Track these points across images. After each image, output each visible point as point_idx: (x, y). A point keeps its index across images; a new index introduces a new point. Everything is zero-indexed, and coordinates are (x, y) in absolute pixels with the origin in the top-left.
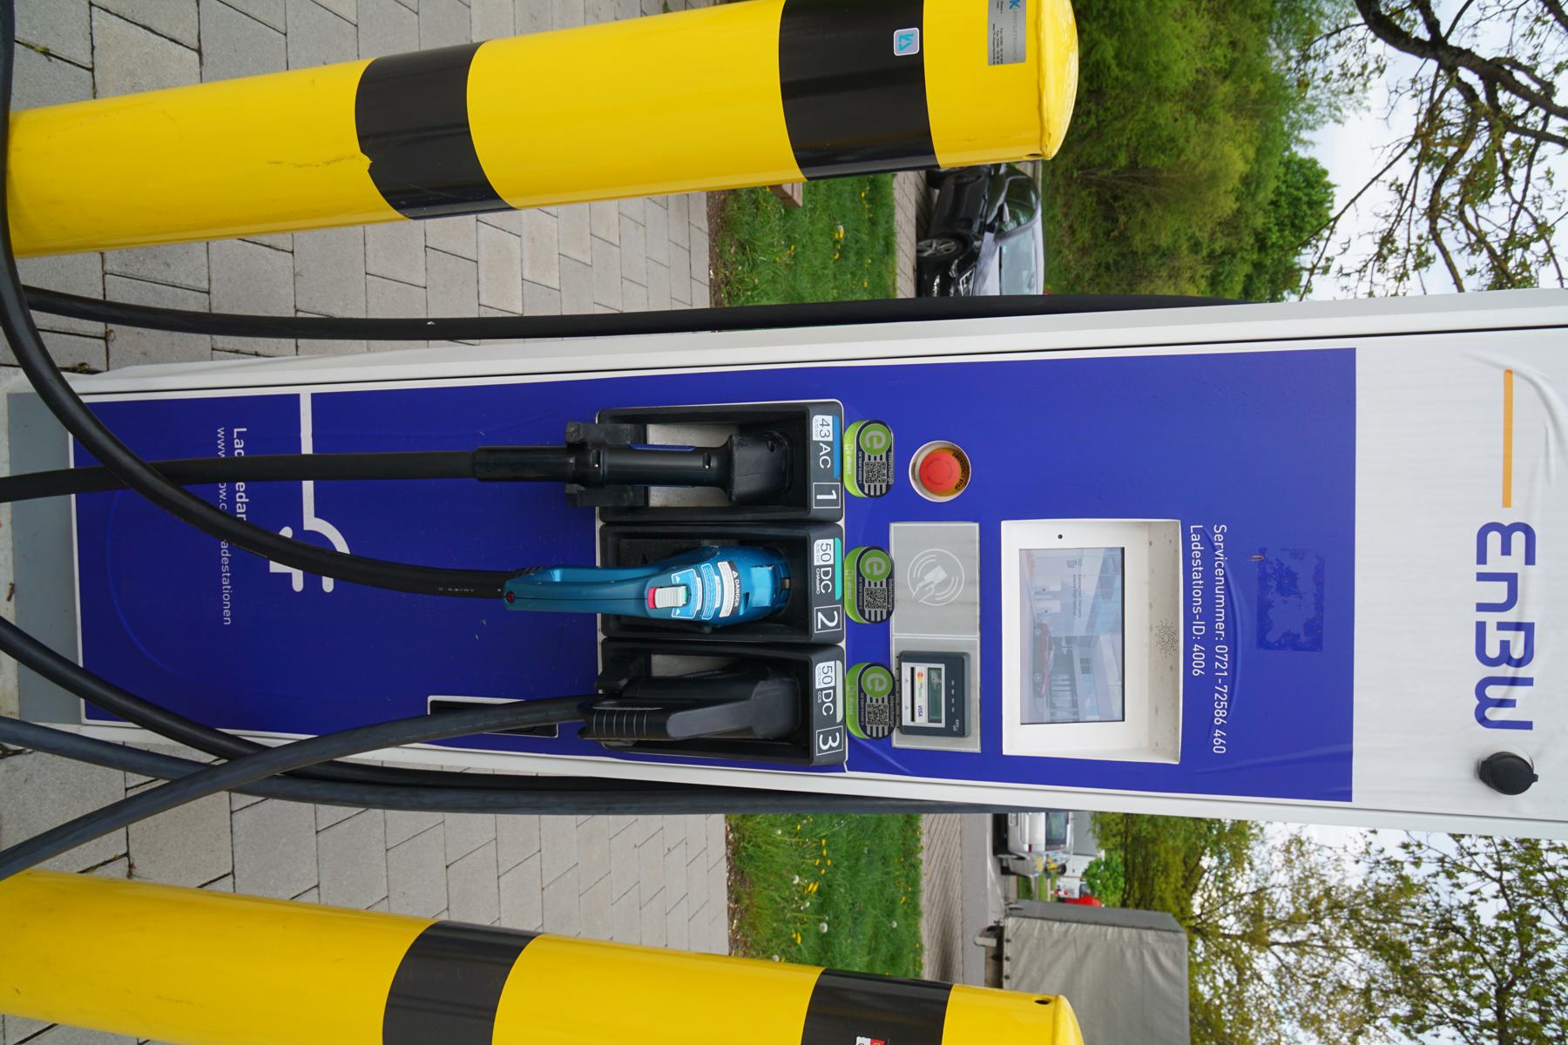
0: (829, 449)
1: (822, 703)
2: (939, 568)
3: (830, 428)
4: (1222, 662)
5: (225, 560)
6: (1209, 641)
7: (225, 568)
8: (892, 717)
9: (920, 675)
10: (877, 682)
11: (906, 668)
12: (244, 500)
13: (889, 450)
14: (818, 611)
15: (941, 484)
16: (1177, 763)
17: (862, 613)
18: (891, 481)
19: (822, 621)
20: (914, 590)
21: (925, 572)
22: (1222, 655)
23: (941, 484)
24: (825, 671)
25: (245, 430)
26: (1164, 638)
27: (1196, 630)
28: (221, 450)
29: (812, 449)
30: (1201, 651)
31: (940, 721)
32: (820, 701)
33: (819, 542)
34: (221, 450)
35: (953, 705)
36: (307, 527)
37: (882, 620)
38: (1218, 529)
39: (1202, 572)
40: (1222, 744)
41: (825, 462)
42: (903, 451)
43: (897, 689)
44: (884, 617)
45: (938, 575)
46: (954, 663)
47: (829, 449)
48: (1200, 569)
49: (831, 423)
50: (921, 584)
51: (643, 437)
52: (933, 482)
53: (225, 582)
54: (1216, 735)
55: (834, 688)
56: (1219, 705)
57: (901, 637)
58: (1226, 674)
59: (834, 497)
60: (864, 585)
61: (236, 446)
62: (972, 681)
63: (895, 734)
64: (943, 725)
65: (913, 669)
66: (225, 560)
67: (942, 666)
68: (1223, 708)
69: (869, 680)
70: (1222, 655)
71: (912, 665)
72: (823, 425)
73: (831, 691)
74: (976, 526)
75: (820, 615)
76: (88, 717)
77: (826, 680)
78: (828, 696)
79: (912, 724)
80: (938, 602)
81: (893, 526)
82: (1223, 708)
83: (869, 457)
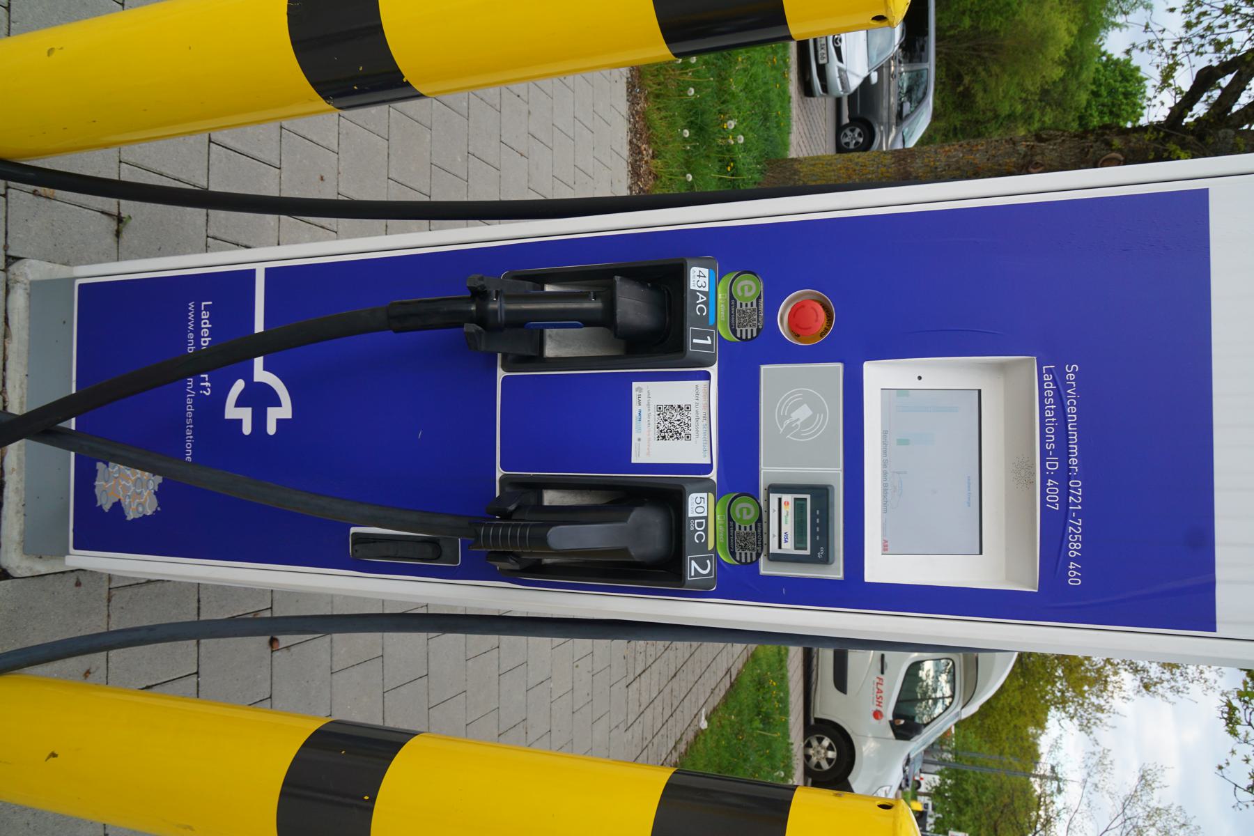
0: (705, 299)
1: (695, 531)
2: (805, 406)
3: (707, 280)
4: (1075, 496)
5: (189, 414)
6: (1064, 476)
7: (189, 421)
8: (759, 543)
9: (787, 503)
10: (744, 510)
11: (774, 498)
12: (208, 326)
13: (759, 297)
14: (691, 559)
15: (810, 328)
16: (1036, 591)
17: (734, 332)
18: (760, 327)
19: (695, 568)
20: (782, 427)
21: (791, 411)
22: (1075, 489)
23: (810, 328)
24: (698, 501)
25: (210, 303)
26: (1018, 473)
27: (1050, 465)
28: (191, 311)
29: (689, 300)
30: (1055, 485)
31: (806, 549)
32: (692, 529)
33: (694, 269)
34: (191, 311)
35: (818, 517)
36: (256, 379)
37: (752, 562)
38: (1069, 369)
39: (1054, 410)
40: (1077, 576)
41: (701, 310)
42: (771, 300)
43: (764, 519)
44: (754, 559)
45: (803, 413)
46: (821, 494)
47: (705, 299)
48: (1053, 407)
49: (707, 275)
50: (788, 421)
51: (540, 498)
52: (801, 328)
53: (189, 433)
54: (1071, 567)
55: (706, 518)
56: (1074, 538)
57: (769, 470)
58: (1080, 508)
59: (709, 342)
60: (734, 529)
61: (203, 317)
62: (836, 547)
63: (762, 560)
64: (808, 552)
65: (780, 500)
66: (189, 414)
67: (808, 497)
68: (1078, 541)
69: (739, 289)
70: (1075, 489)
71: (779, 495)
72: (699, 276)
73: (704, 521)
74: (840, 366)
75: (694, 563)
76: (76, 547)
77: (699, 510)
78: (700, 525)
79: (779, 551)
80: (800, 392)
81: (764, 368)
82: (1078, 541)
83: (740, 527)
